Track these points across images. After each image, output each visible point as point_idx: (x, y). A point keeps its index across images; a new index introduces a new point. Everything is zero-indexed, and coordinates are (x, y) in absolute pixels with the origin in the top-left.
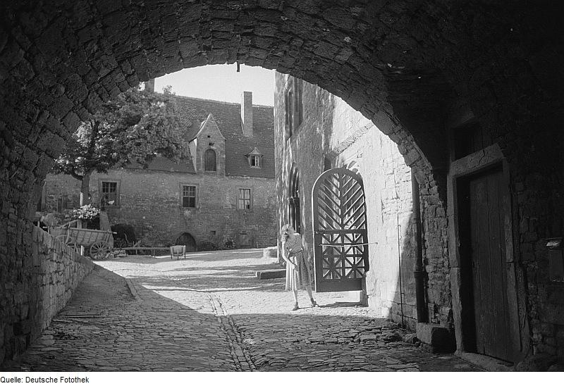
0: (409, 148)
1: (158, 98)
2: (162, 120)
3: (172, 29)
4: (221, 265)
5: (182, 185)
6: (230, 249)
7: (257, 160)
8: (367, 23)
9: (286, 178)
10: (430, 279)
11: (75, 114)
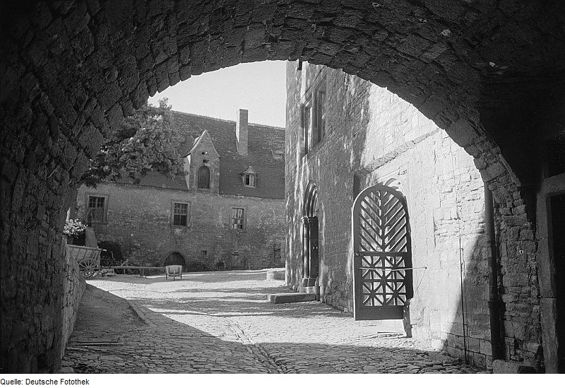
0: (491, 161)
1: (153, 111)
2: (160, 134)
3: (247, 10)
4: (224, 287)
5: (173, 202)
6: (221, 270)
7: (251, 180)
8: (479, 12)
9: (300, 199)
10: (508, 309)
11: (120, 106)
